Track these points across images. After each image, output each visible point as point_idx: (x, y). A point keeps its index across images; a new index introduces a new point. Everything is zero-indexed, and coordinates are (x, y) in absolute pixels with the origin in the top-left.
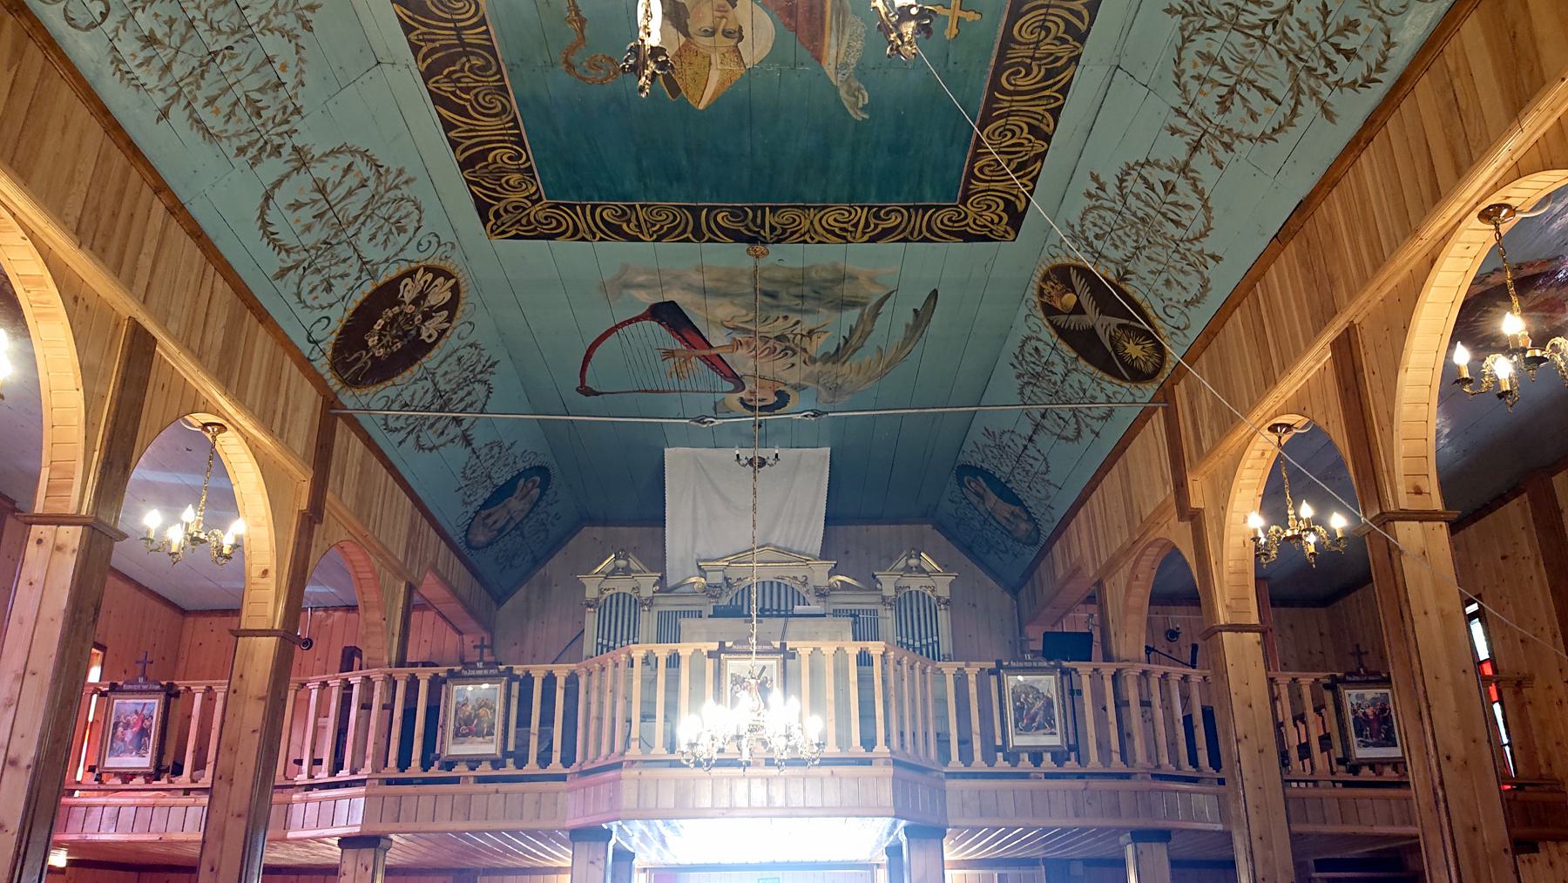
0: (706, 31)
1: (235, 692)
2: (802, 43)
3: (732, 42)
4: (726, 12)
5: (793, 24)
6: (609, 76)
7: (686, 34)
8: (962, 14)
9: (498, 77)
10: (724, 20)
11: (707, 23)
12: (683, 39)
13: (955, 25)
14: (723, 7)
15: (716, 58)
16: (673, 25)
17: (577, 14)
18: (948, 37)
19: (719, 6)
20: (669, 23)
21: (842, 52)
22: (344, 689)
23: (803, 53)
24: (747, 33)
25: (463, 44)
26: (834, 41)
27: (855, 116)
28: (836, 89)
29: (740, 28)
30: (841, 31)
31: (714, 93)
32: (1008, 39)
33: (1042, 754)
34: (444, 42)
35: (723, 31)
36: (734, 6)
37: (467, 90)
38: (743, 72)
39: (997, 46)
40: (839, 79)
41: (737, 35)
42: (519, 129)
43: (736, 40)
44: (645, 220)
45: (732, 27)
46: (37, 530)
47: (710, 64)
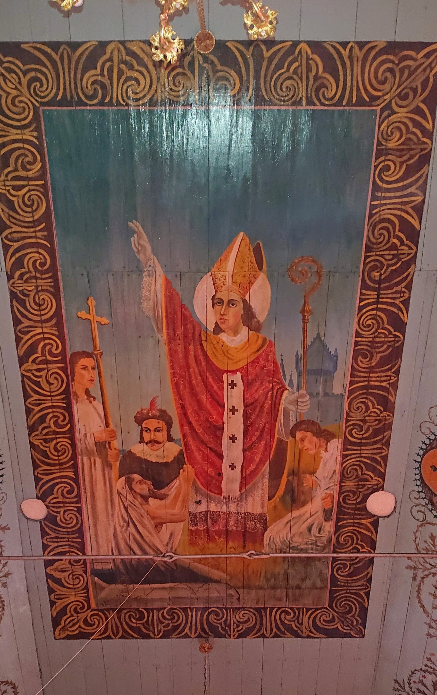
0: (233, 304)
1: (188, 664)
2: (178, 294)
3: (219, 295)
4: (221, 319)
5: (183, 310)
6: (297, 264)
7: (244, 301)
8: (88, 317)
9: (363, 297)
10: (222, 313)
11: (232, 310)
12: (247, 298)
13: (91, 308)
14: (222, 323)
15: (229, 281)
16: (252, 309)
17: (304, 317)
18: (92, 298)
19: (224, 323)
20: (253, 310)
21: (153, 287)
22: (230, 637)
23: (176, 285)
24: (210, 302)
25: (378, 290)
26: (159, 295)
27: (138, 224)
28: (154, 252)
29: (213, 307)
30: (156, 304)
31: (233, 247)
32: (56, 294)
33: (332, 393)
34: (391, 291)
35: (223, 304)
36: (216, 323)
37: (394, 247)
38: (213, 270)
39: (62, 290)
40: (152, 262)
41: (215, 302)
42: (361, 292)
43: (216, 297)
44: (301, 79)
45: (218, 307)
46: (326, 442)
47: (232, 276)
